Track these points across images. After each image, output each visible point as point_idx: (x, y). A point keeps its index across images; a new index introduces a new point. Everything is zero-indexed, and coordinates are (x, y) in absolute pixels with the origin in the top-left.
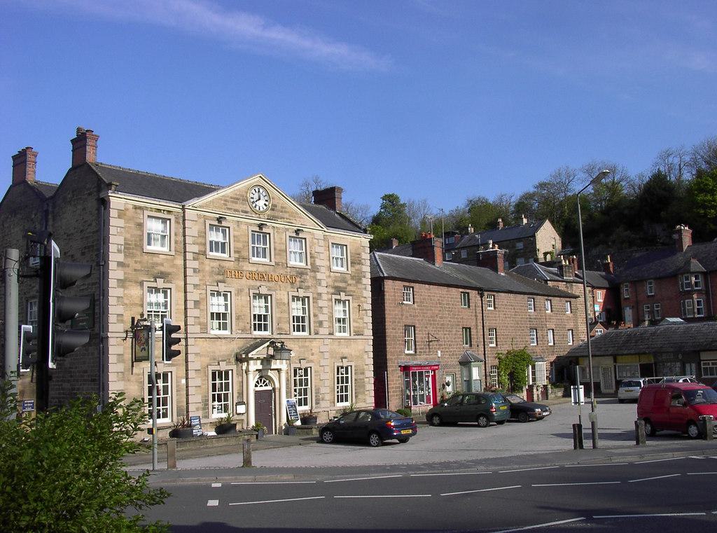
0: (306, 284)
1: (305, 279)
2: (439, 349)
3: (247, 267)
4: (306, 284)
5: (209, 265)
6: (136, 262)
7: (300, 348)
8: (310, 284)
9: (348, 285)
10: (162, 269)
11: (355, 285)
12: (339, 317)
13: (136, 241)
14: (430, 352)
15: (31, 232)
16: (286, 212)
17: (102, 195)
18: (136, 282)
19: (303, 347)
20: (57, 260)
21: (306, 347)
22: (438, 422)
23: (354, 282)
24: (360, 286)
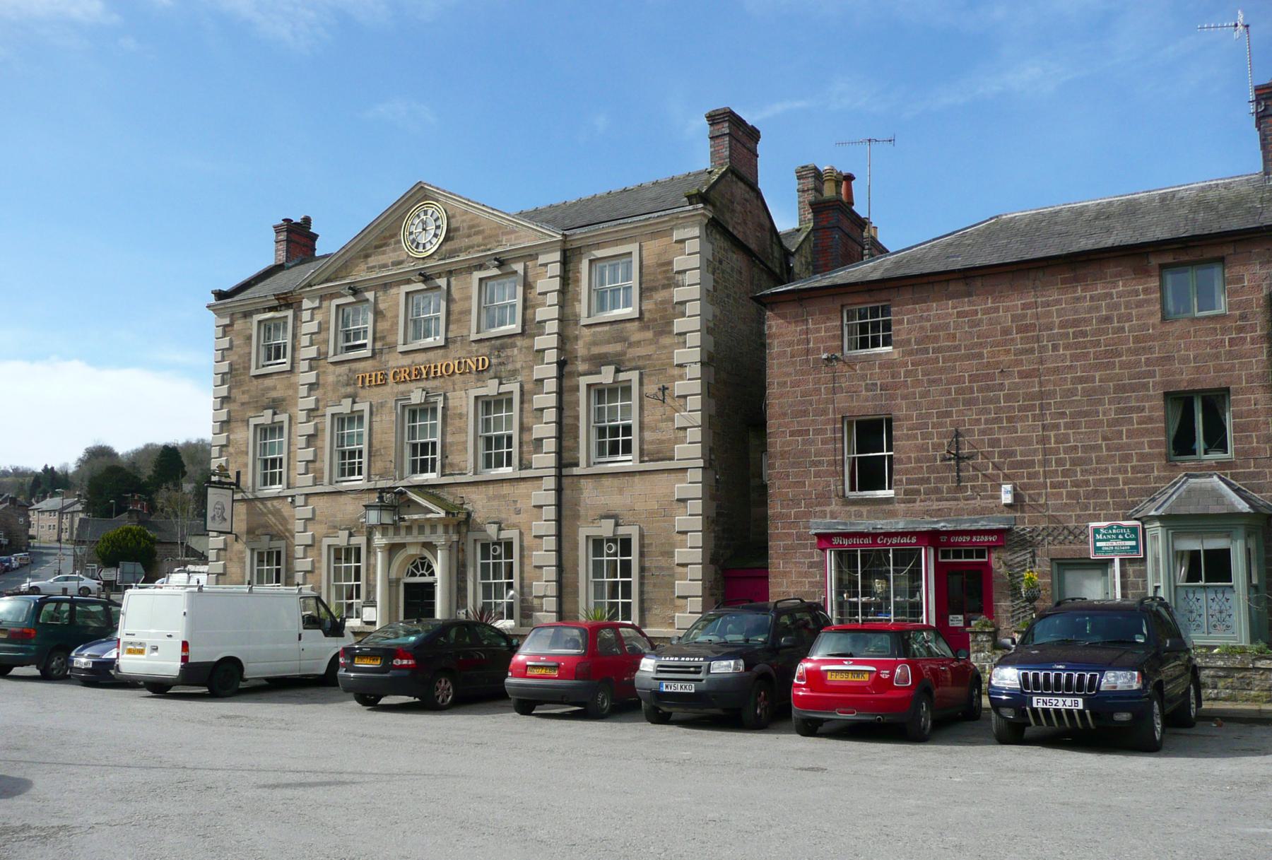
0: (510, 367)
1: (508, 357)
2: (1007, 478)
3: (395, 361)
4: (510, 367)
5: (334, 374)
6: (243, 393)
7: (489, 499)
8: (518, 365)
9: (631, 345)
10: (274, 394)
11: (654, 342)
12: (412, 399)
13: (244, 362)
14: (959, 489)
15: (1215, 654)
16: (477, 233)
17: (443, 275)
18: (243, 421)
19: (495, 497)
20: (812, 691)
21: (504, 496)
22: (883, 676)
23: (649, 335)
24: (666, 340)
